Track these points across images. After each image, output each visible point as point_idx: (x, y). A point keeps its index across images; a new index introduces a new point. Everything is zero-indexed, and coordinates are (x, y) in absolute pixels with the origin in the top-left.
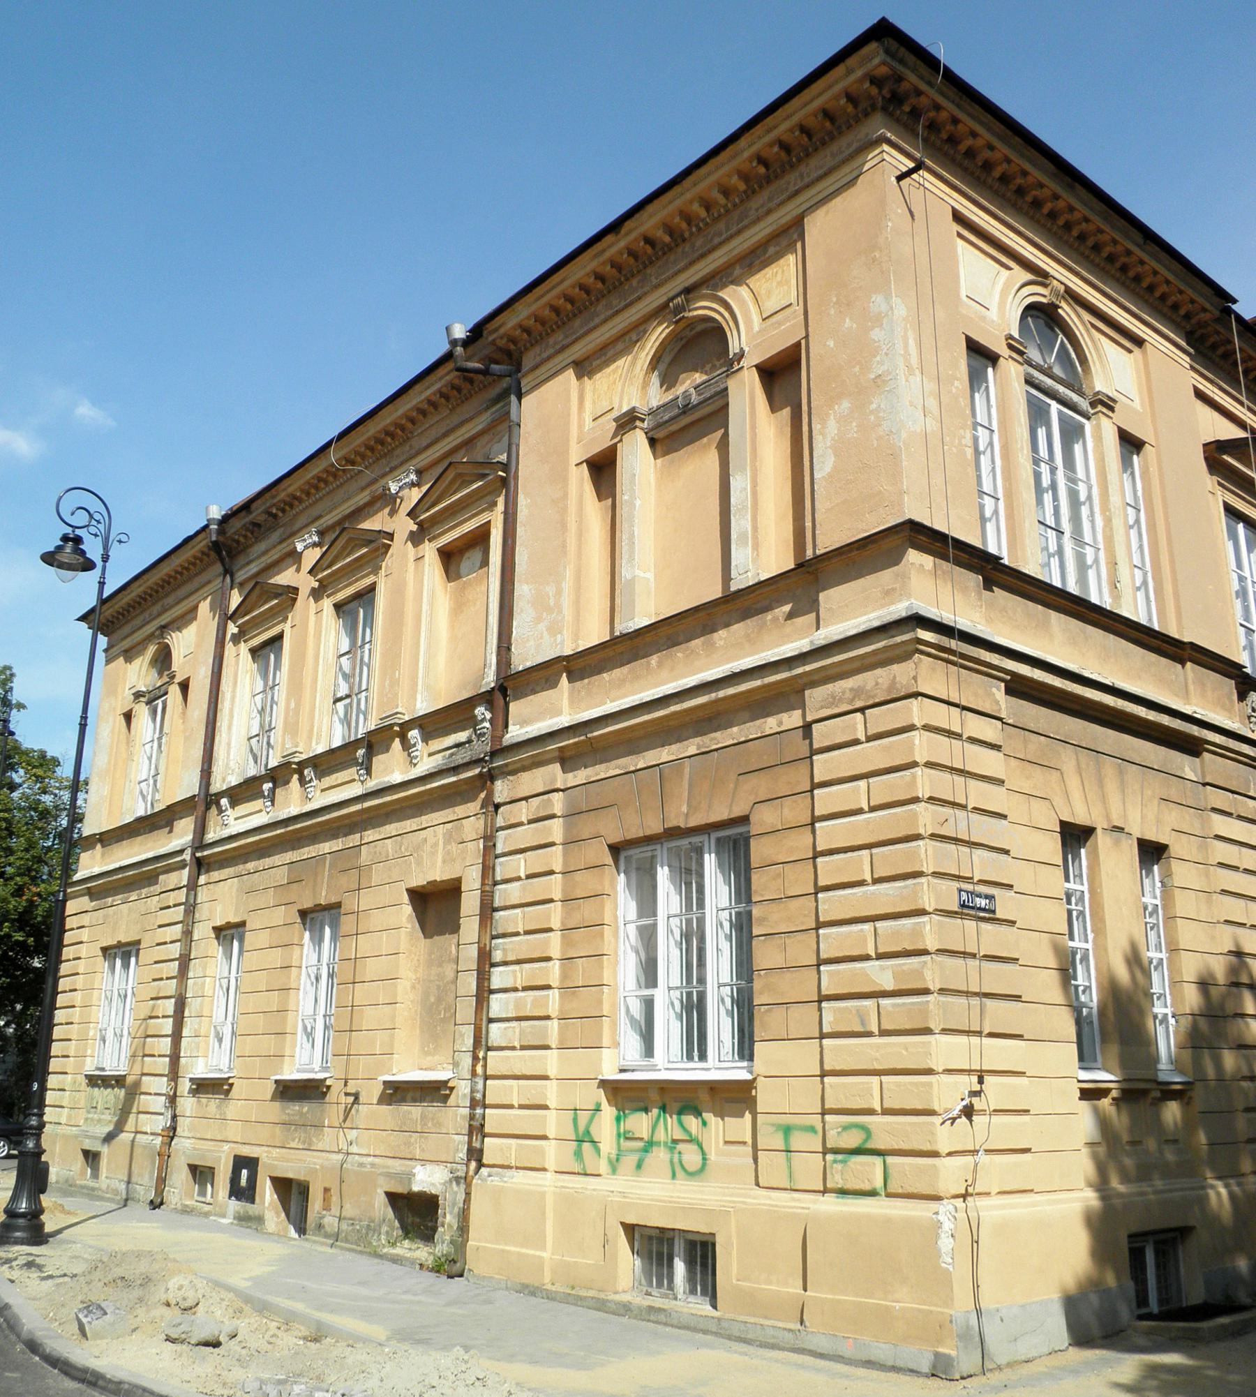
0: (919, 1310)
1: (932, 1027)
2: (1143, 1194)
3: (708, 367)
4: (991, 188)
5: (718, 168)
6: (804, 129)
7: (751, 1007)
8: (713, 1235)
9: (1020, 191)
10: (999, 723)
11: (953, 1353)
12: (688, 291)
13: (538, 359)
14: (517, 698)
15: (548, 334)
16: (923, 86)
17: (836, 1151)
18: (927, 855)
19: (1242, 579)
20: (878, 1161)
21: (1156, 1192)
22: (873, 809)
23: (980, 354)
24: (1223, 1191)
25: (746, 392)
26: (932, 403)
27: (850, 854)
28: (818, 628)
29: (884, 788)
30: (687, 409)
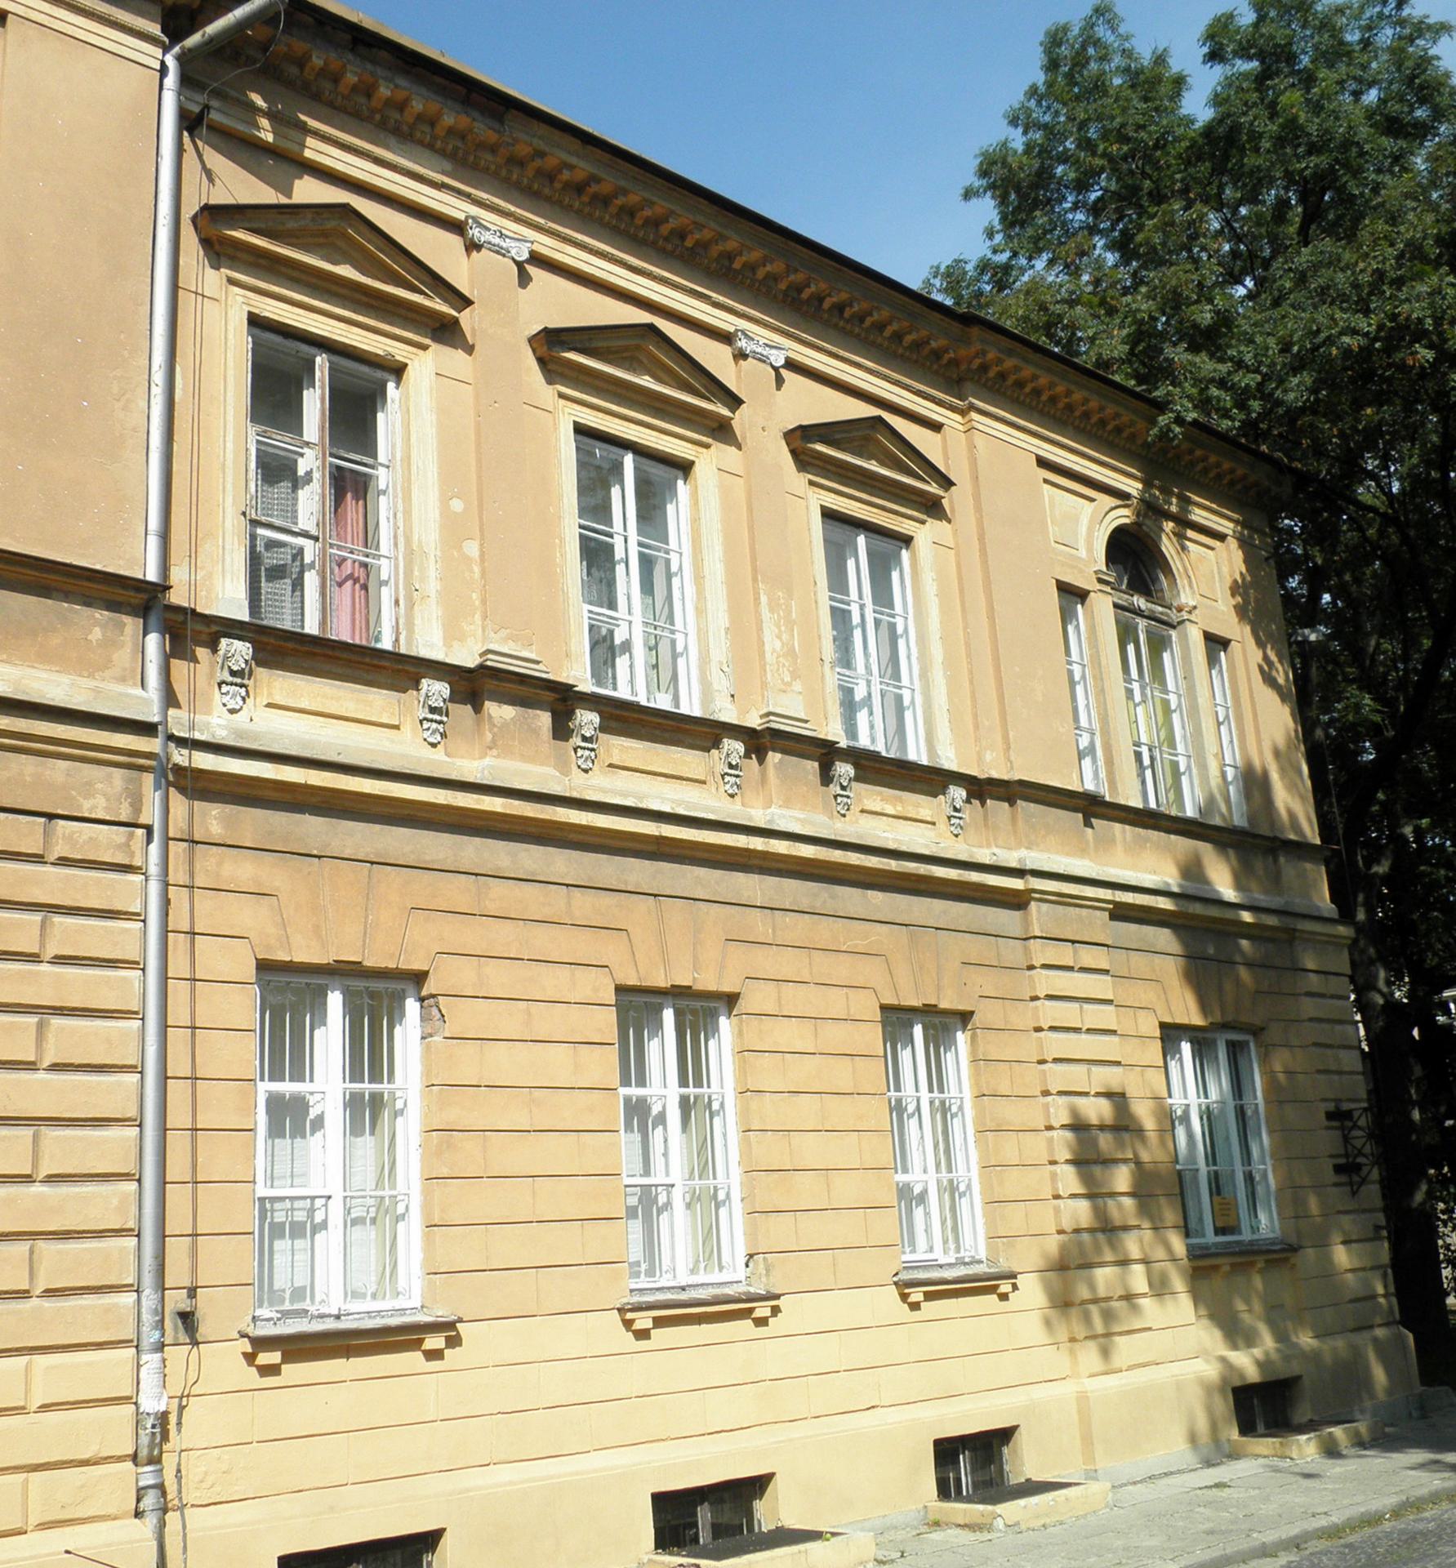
23: (1071, 594)
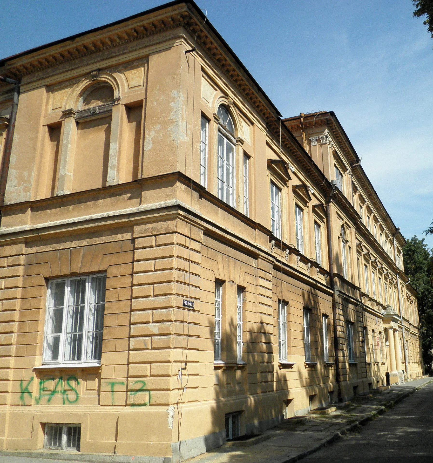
0: (159, 443)
1: (171, 346)
2: (229, 400)
3: (104, 100)
4: (214, 62)
5: (118, 29)
6: (154, 25)
7: (101, 340)
8: (80, 424)
9: (223, 66)
10: (200, 244)
11: (171, 457)
12: (99, 70)
13: (29, 80)
14: (6, 215)
15: (35, 72)
16: (198, 23)
17: (131, 391)
18: (175, 288)
19: (273, 204)
20: (147, 393)
21: (233, 400)
22: (156, 271)
23: (205, 118)
24: (252, 399)
25: (119, 114)
26: (189, 132)
27: (146, 286)
28: (140, 204)
29: (160, 264)
30: (94, 114)
